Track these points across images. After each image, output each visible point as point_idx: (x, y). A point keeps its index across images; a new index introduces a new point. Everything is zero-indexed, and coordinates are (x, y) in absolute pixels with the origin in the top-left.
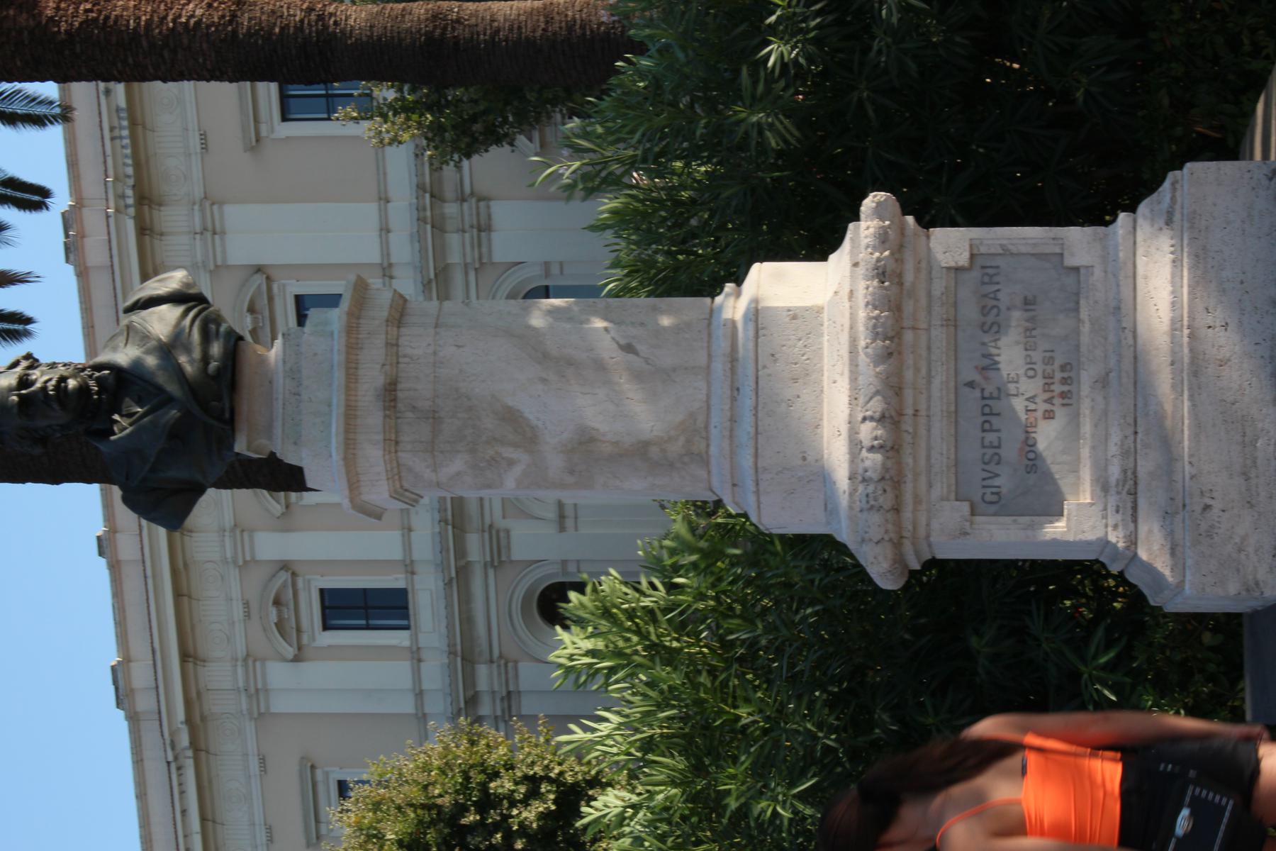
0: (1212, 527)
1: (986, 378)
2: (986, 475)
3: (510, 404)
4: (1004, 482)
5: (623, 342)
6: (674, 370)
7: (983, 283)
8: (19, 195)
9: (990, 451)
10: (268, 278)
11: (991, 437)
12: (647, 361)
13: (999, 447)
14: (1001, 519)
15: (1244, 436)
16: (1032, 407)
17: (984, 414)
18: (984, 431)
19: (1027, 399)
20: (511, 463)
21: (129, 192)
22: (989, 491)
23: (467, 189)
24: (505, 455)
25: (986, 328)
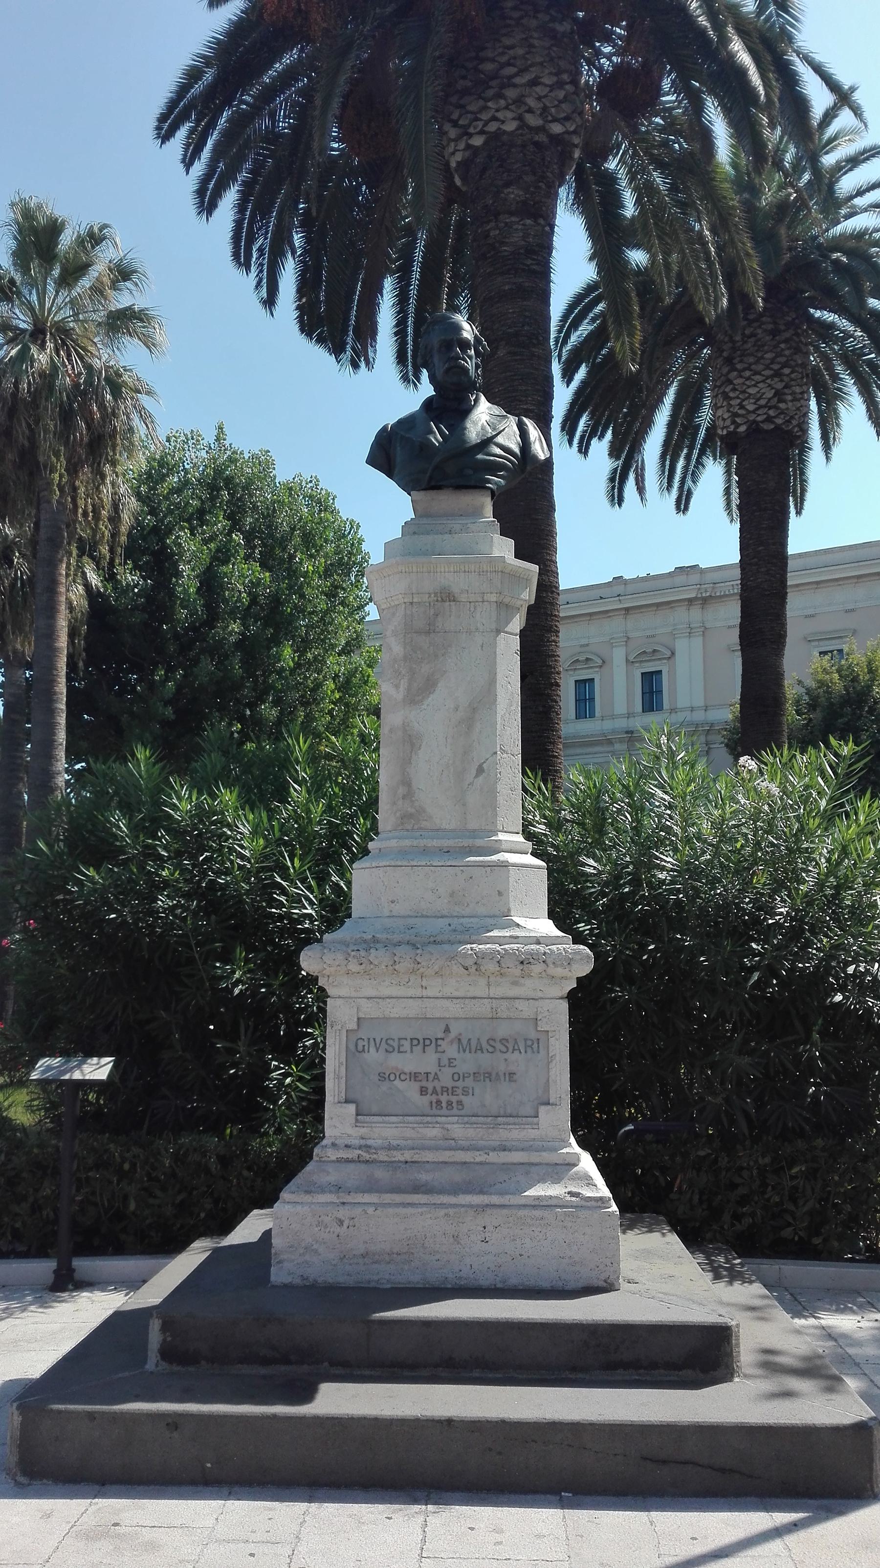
0: (326, 1227)
1: (452, 1042)
2: (378, 1041)
4: (373, 1056)
5: (485, 765)
6: (464, 805)
7: (526, 1040)
8: (684, 498)
9: (395, 1044)
11: (407, 1045)
12: (471, 784)
13: (399, 1052)
14: (344, 1054)
15: (398, 1254)
16: (431, 1077)
19: (436, 1074)
20: (397, 687)
22: (366, 1043)
23: (712, 746)
25: (491, 1042)
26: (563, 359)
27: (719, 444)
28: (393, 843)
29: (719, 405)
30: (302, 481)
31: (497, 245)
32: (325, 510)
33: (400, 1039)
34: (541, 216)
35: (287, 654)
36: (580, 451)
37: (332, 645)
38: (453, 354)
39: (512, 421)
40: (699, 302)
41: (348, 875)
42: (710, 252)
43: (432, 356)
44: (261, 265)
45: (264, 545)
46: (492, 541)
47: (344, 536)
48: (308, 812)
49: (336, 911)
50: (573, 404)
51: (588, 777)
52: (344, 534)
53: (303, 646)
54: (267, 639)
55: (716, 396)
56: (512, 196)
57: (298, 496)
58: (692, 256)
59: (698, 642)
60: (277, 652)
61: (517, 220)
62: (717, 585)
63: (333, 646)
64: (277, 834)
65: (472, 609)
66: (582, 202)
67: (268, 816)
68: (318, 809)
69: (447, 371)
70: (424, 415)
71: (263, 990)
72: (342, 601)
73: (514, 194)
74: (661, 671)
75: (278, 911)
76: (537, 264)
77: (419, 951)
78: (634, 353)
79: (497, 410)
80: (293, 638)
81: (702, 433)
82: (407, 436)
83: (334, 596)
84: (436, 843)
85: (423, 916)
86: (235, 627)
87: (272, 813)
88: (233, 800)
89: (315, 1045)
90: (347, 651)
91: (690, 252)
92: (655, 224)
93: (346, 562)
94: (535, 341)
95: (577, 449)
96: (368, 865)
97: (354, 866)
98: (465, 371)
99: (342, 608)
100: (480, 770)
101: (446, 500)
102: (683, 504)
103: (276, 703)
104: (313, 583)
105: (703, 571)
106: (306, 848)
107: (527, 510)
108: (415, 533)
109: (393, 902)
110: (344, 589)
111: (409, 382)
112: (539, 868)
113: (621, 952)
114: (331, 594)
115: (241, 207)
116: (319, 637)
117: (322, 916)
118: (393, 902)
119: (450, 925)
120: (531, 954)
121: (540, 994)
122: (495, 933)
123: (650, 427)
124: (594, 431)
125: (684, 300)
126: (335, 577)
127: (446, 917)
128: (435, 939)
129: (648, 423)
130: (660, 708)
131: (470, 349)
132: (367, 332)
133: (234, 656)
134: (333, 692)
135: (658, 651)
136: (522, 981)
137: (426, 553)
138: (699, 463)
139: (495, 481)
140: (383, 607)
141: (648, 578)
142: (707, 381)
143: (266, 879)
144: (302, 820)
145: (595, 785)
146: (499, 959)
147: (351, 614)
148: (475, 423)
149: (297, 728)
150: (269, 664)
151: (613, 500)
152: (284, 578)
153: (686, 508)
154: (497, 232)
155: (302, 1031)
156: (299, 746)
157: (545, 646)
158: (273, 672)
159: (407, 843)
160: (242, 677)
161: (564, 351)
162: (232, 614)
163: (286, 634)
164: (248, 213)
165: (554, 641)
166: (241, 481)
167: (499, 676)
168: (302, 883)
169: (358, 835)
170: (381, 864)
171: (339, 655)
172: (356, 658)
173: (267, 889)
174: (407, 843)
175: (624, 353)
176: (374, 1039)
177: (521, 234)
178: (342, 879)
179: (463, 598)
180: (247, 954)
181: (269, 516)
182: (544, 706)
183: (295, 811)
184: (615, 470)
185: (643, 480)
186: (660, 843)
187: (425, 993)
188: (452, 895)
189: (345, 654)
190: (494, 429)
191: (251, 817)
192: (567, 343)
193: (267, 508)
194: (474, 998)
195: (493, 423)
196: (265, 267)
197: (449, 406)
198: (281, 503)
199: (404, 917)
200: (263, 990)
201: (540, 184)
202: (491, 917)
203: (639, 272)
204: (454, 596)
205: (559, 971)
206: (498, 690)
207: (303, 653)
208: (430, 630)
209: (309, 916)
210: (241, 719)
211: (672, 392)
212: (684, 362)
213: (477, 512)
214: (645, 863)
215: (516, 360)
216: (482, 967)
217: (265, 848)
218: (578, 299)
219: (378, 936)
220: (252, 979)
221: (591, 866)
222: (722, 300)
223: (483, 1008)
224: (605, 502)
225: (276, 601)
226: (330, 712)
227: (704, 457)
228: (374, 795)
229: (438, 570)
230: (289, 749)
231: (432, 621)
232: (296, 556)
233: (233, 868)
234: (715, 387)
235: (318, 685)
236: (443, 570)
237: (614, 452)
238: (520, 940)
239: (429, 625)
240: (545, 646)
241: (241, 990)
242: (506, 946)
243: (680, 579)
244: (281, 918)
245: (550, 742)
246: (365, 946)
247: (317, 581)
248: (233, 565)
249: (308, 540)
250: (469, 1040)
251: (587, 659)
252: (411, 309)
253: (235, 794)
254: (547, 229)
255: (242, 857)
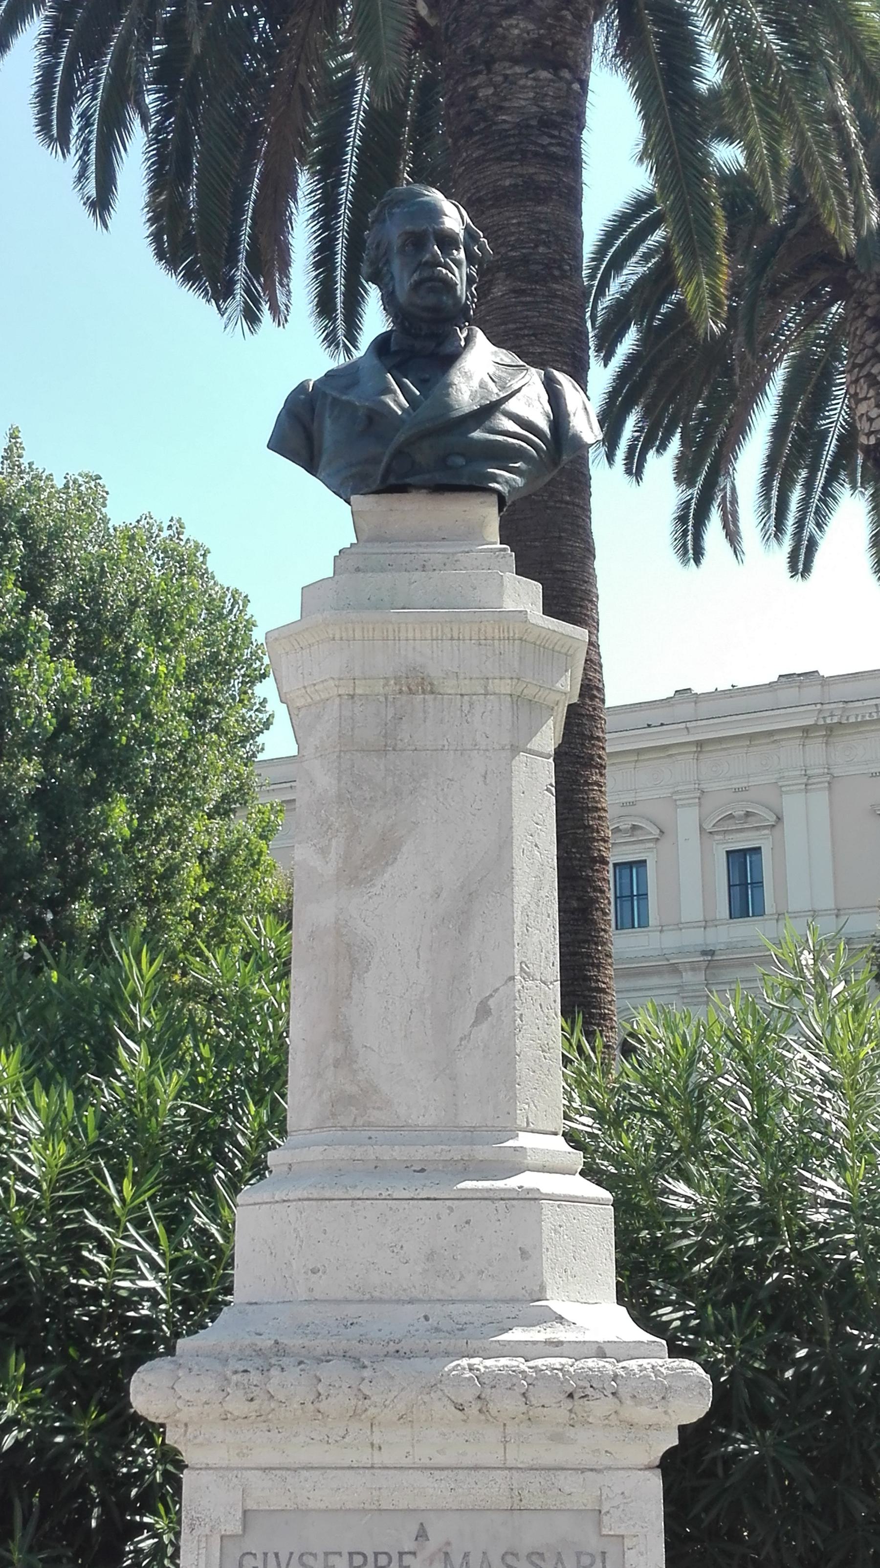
3: (404, 849)
5: (492, 1003)
6: (453, 1078)
7: (579, 1554)
10: (773, 826)
17: (376, 1554)
18: (351, 1554)
20: (323, 852)
21: (835, 720)
24: (334, 843)
26: (599, 320)
27: (860, 461)
28: (314, 1154)
29: (860, 396)
30: (152, 526)
31: (490, 112)
32: (190, 573)
33: (326, 1554)
34: (566, 66)
35: (120, 815)
36: (629, 471)
37: (198, 799)
38: (427, 257)
39: (533, 378)
40: (829, 220)
41: (226, 1213)
42: (849, 135)
43: (388, 262)
44: (87, 142)
45: (83, 630)
46: (502, 584)
47: (221, 617)
48: (151, 1090)
49: (202, 1288)
50: (612, 395)
51: (671, 1027)
52: (221, 614)
53: (145, 807)
54: (87, 789)
55: (856, 381)
56: (516, 32)
57: (144, 549)
58: (817, 143)
59: (820, 799)
60: (102, 812)
61: (525, 70)
62: (851, 705)
63: (199, 802)
64: (93, 1134)
65: (466, 708)
66: (630, 50)
67: (77, 1101)
68: (169, 1085)
69: (416, 287)
70: (376, 362)
71: (59, 1439)
72: (217, 725)
73: (519, 28)
74: (759, 848)
75: (92, 1283)
76: (559, 144)
77: (367, 1373)
78: (717, 303)
79: (507, 357)
80: (130, 789)
81: (831, 445)
82: (344, 398)
83: (203, 717)
84: (398, 1153)
85: (372, 1300)
86: (31, 768)
87: (83, 1093)
88: (11, 1070)
89: (158, 1551)
90: (222, 810)
91: (814, 135)
92: (755, 89)
93: (223, 664)
94: (556, 273)
95: (623, 468)
96: (266, 1197)
97: (239, 1198)
98: (450, 286)
99: (215, 737)
100: (483, 1011)
101: (415, 511)
102: (801, 561)
103: (99, 900)
104: (167, 696)
105: (826, 682)
106: (147, 1158)
107: (554, 547)
108: (358, 570)
109: (314, 1271)
110: (219, 705)
111: (337, 346)
112: (599, 1202)
113: (744, 1364)
114: (197, 714)
115: (51, 44)
116: (175, 786)
117: (174, 1294)
118: (314, 1271)
119: (426, 1318)
120: (588, 1377)
121: (605, 1460)
122: (517, 1335)
123: (743, 433)
124: (652, 438)
125: (802, 221)
126: (205, 684)
127: (419, 1301)
128: (397, 1347)
129: (740, 428)
130: (760, 912)
131: (458, 249)
132: (270, 261)
133: (27, 818)
134: (198, 880)
135: (754, 814)
136: (571, 1433)
137: (378, 606)
138: (827, 494)
139: (506, 479)
140: (300, 703)
141: (734, 692)
142: (840, 359)
143: (69, 1220)
144: (138, 1108)
145: (685, 1043)
146: (526, 1388)
147: (232, 747)
148: (468, 376)
149: (137, 938)
150: (88, 832)
151: (686, 552)
152: (117, 686)
153: (807, 569)
154: (491, 91)
155: (133, 1521)
156: (140, 970)
157: (582, 792)
158: (95, 846)
159: (342, 1152)
160: (41, 855)
161: (600, 307)
162: (27, 745)
163: (118, 782)
164: (63, 55)
165: (597, 783)
166: (47, 524)
167: (518, 833)
168: (137, 1227)
169: (244, 1134)
170: (291, 1196)
171: (210, 817)
172: (239, 823)
173: (70, 1242)
174: (342, 1152)
175: (700, 303)
176: (276, 1555)
177: (531, 95)
178: (213, 1221)
179: (449, 687)
180: (31, 1366)
181: (93, 588)
182: (579, 899)
183: (127, 1092)
184: (687, 503)
185: (735, 520)
186: (806, 1151)
187: (378, 1459)
188: (431, 1256)
189: (219, 814)
190: (503, 388)
191: (43, 1101)
192: (604, 295)
193: (91, 569)
194: (476, 1468)
195: (500, 377)
196: (93, 145)
197: (422, 346)
198: (115, 561)
199: (337, 1302)
200: (59, 1439)
201: (564, 12)
202: (506, 1301)
203: (724, 179)
204: (431, 684)
205: (644, 1413)
206: (516, 859)
207: (145, 814)
208: (386, 746)
209: (151, 1294)
210: (37, 926)
211: (780, 375)
212: (798, 326)
213: (473, 534)
214: (782, 1193)
215: (525, 304)
216: (491, 1406)
217: (69, 1161)
218: (622, 221)
219: (283, 1340)
220: (37, 1418)
221: (680, 1194)
222: (868, 214)
223: (493, 1490)
224: (672, 558)
225: (102, 724)
226: (193, 916)
227: (835, 484)
228: (275, 1060)
229: (403, 635)
230: (120, 976)
231: (386, 733)
232: (138, 649)
233: (8, 1199)
234: (854, 365)
235: (172, 870)
236: (410, 636)
237: (685, 472)
238: (565, 1349)
239: (385, 736)
240: (582, 792)
241: (17, 1441)
242: (539, 1363)
243: (788, 695)
244: (95, 1295)
245: (593, 965)
246: (259, 1362)
247: (172, 690)
248: (30, 663)
249: (158, 621)
250: (466, 1555)
251: (634, 828)
252: (342, 225)
253: (15, 1058)
254: (576, 86)
255: (25, 1178)
